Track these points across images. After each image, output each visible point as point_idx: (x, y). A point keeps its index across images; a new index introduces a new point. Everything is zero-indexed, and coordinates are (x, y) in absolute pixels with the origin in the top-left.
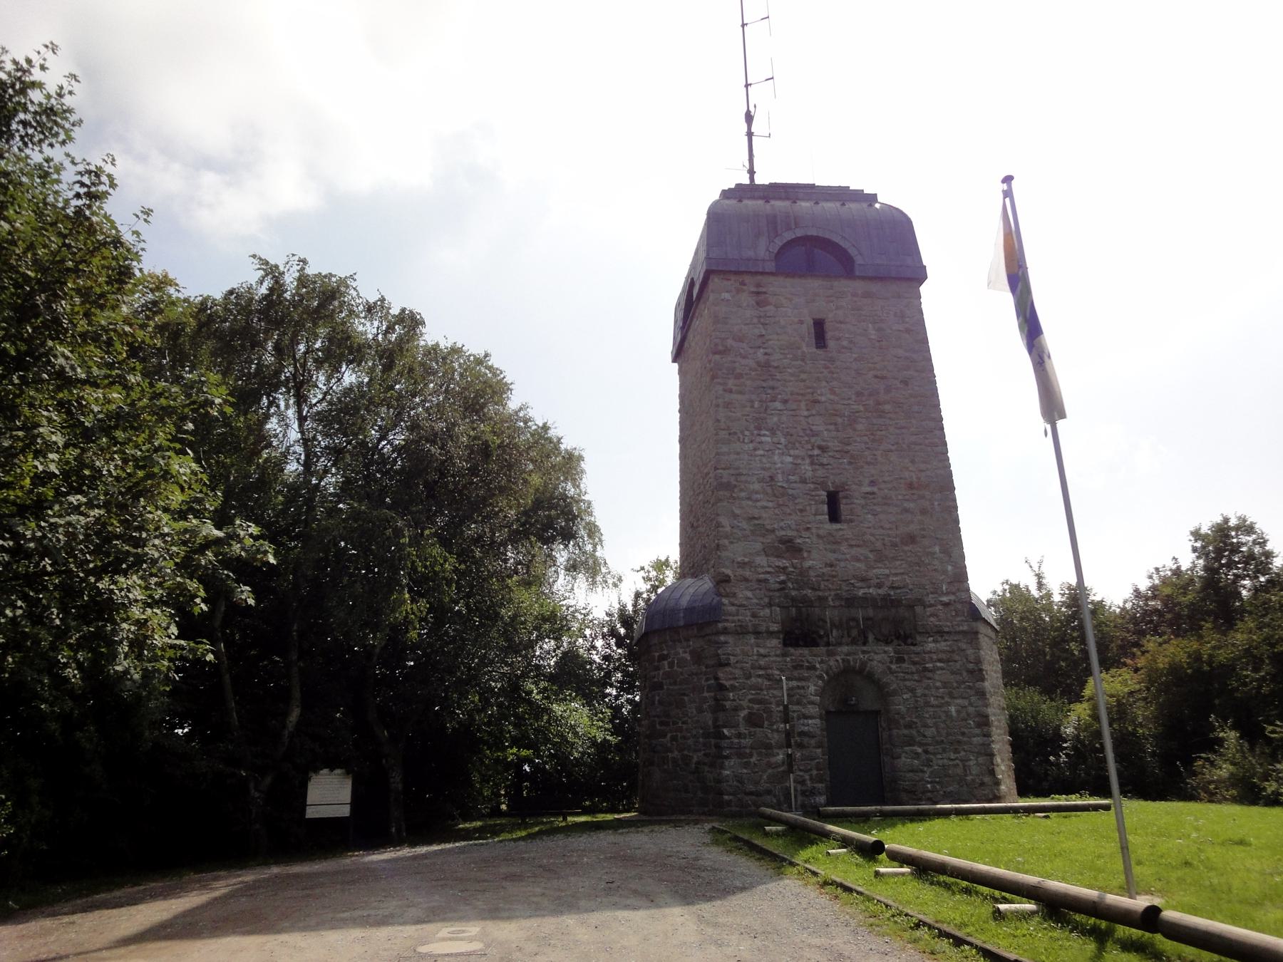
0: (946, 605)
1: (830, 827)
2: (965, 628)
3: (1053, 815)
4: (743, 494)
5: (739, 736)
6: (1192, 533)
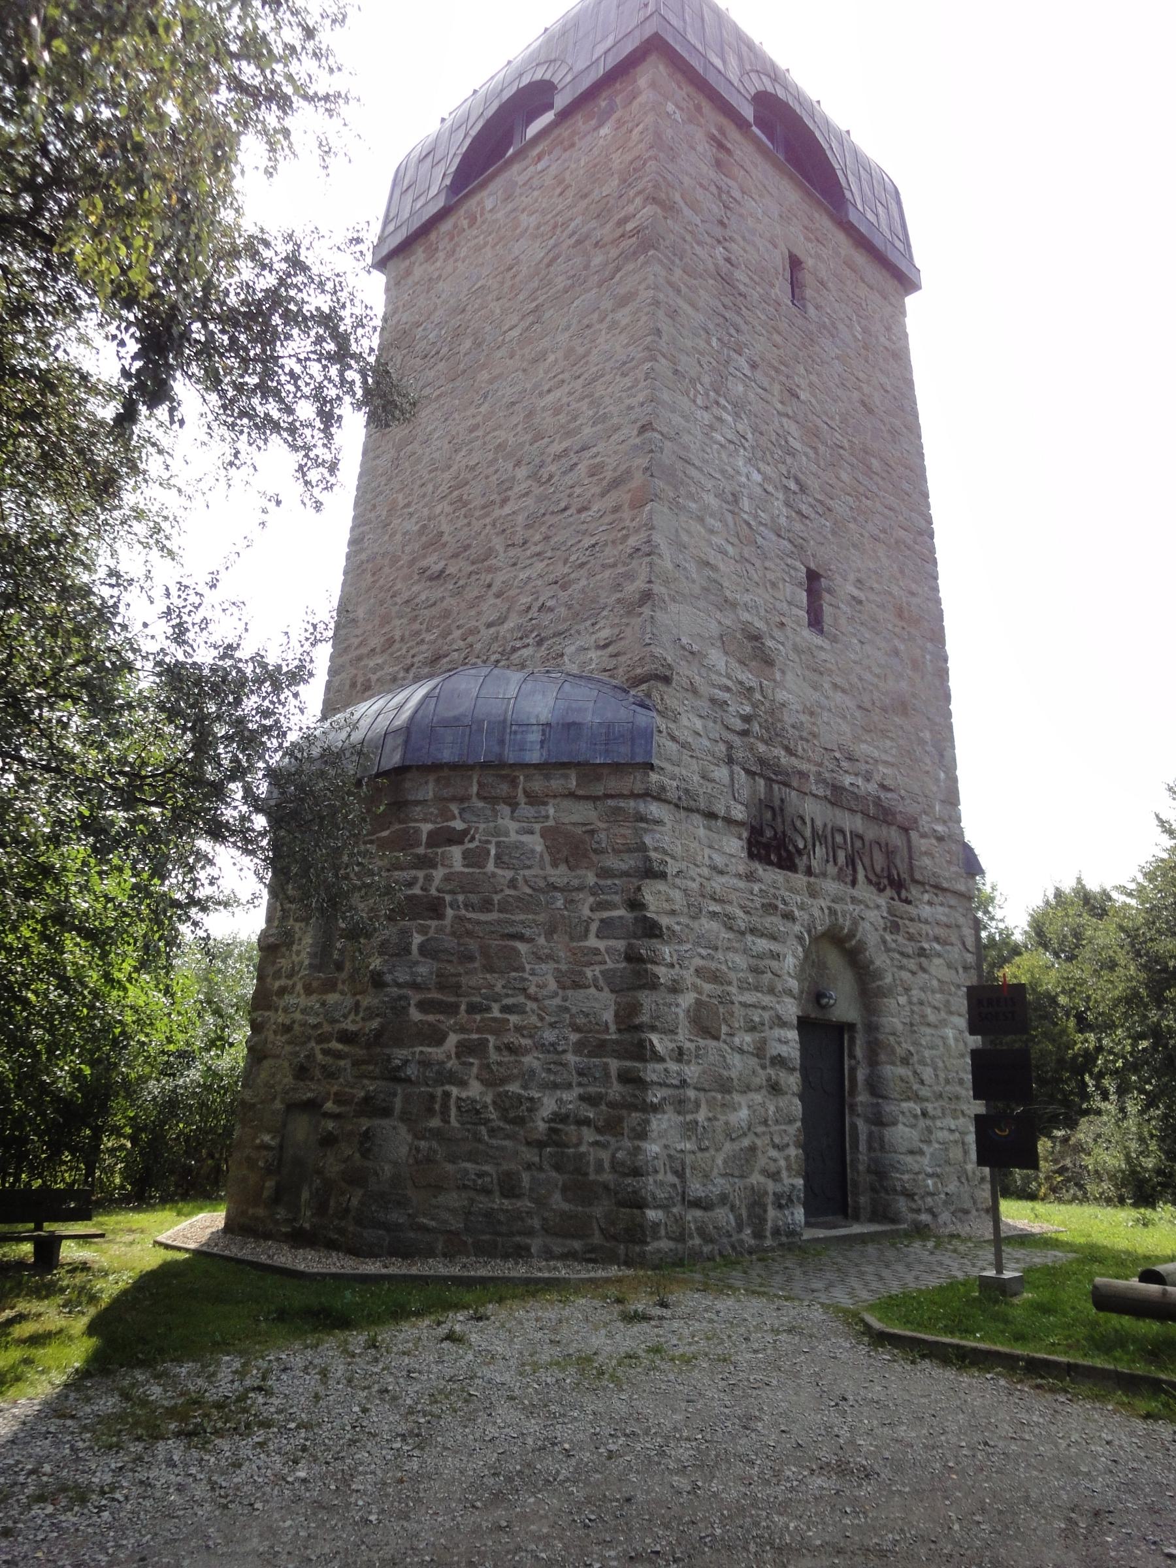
5: (680, 1055)
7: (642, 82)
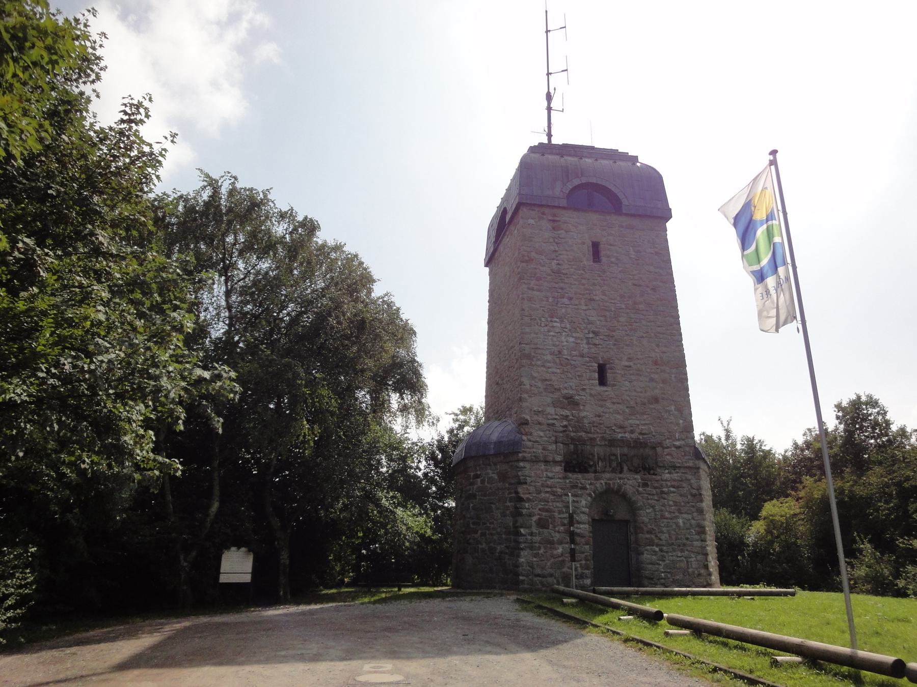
0: (678, 447)
1: (613, 600)
2: (691, 464)
3: (756, 598)
4: (539, 363)
5: (532, 534)
6: (836, 406)
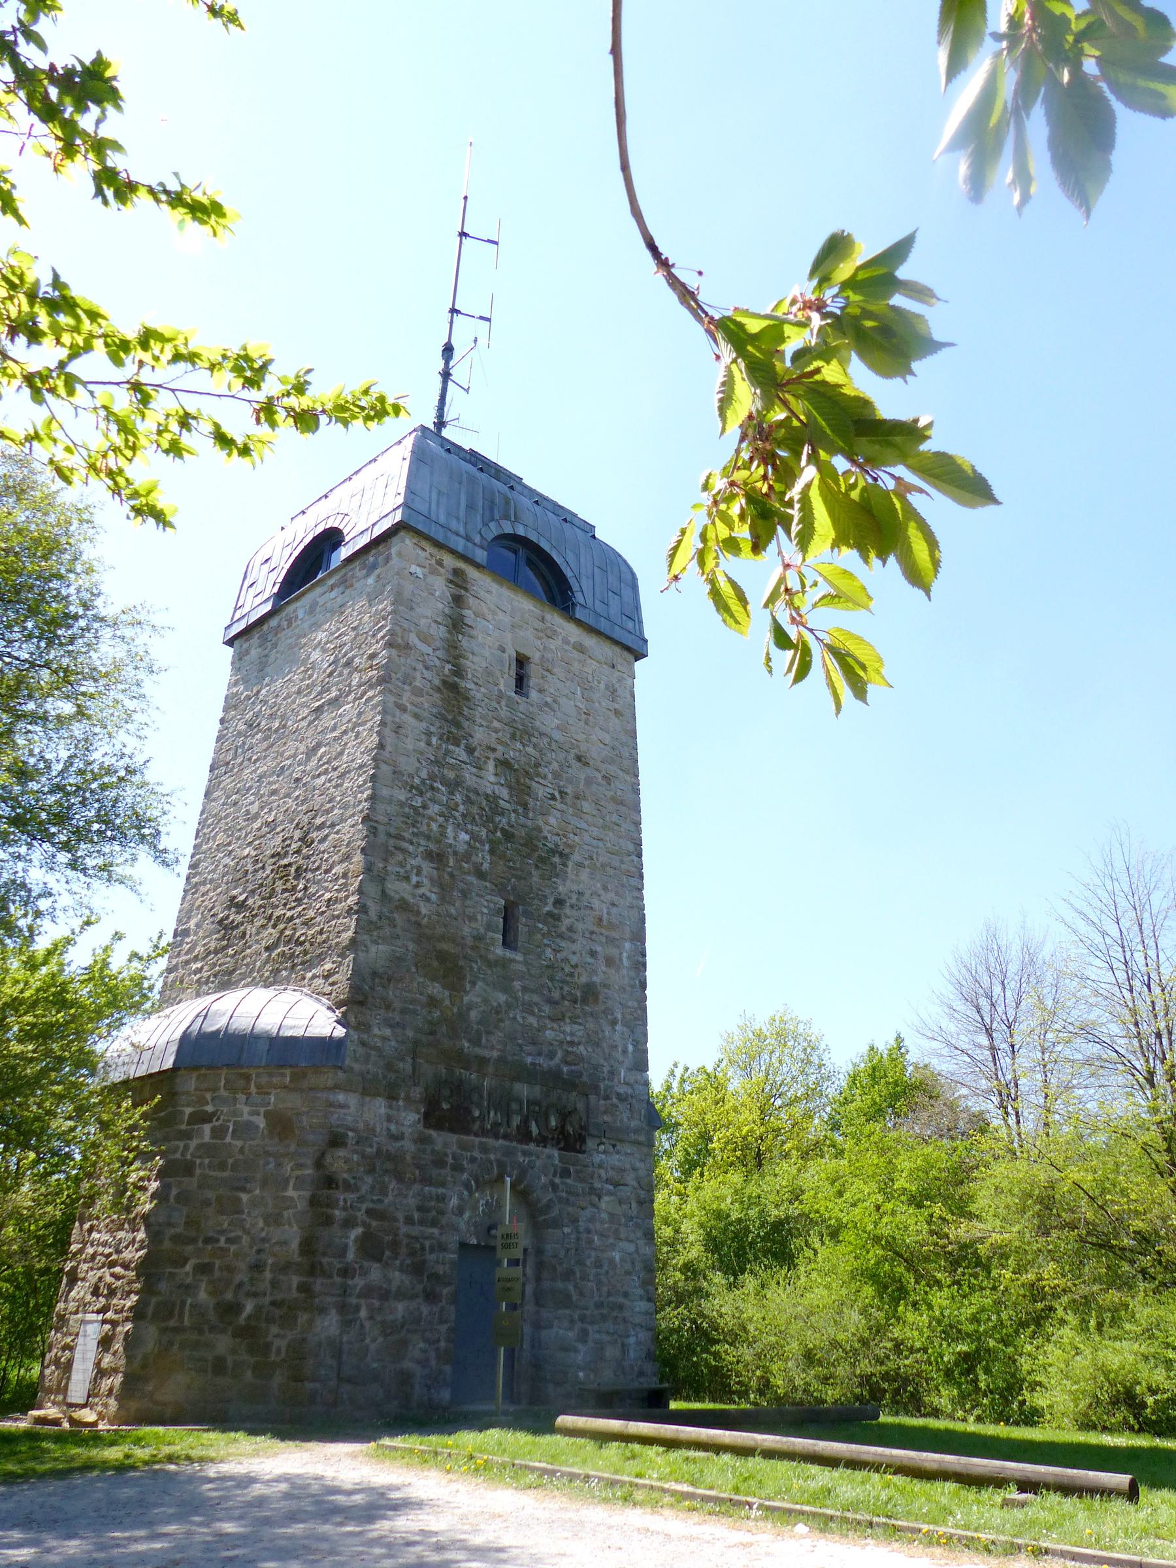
7: (394, 550)
